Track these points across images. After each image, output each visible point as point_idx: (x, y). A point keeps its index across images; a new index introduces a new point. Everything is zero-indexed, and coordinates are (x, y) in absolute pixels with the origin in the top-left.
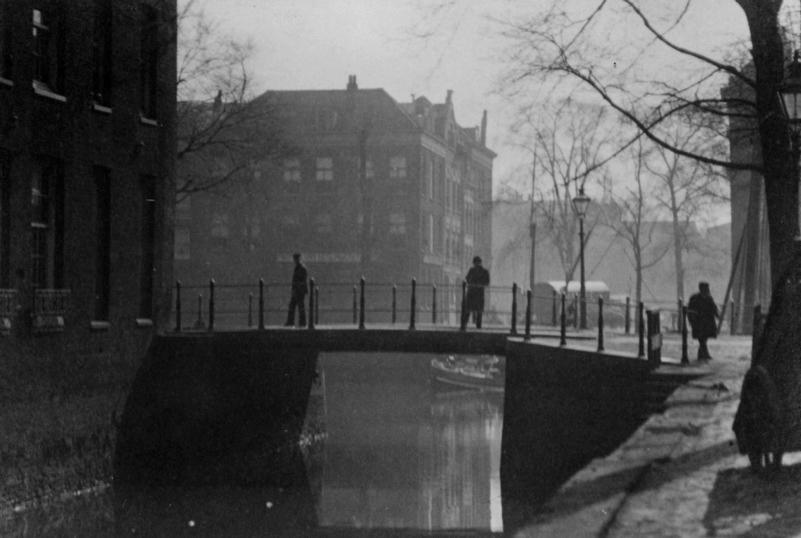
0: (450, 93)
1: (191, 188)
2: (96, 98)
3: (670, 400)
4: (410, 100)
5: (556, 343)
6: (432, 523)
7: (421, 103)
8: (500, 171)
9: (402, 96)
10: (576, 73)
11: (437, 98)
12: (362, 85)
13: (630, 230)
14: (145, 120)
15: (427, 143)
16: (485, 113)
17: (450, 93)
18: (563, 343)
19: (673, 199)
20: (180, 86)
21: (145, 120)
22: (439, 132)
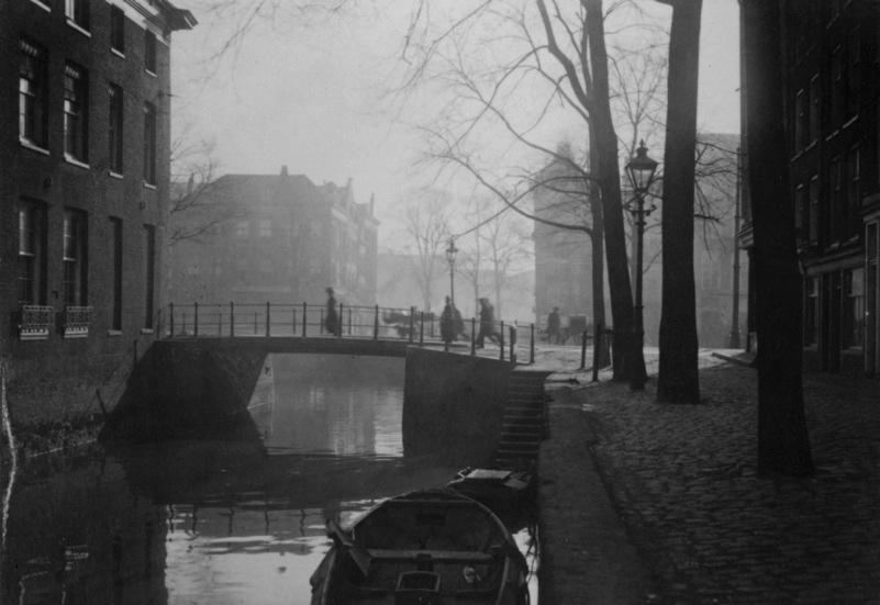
0: (350, 180)
1: (178, 236)
2: (112, 168)
3: (548, 378)
4: (322, 184)
5: (441, 349)
6: (319, 523)
7: (330, 186)
8: (382, 234)
9: (318, 181)
10: (458, 160)
11: (340, 183)
12: (291, 172)
13: (472, 274)
14: (147, 185)
15: (336, 213)
16: (373, 194)
17: (350, 180)
18: (446, 349)
19: (495, 255)
20: (172, 163)
21: (147, 185)
22: (343, 204)
